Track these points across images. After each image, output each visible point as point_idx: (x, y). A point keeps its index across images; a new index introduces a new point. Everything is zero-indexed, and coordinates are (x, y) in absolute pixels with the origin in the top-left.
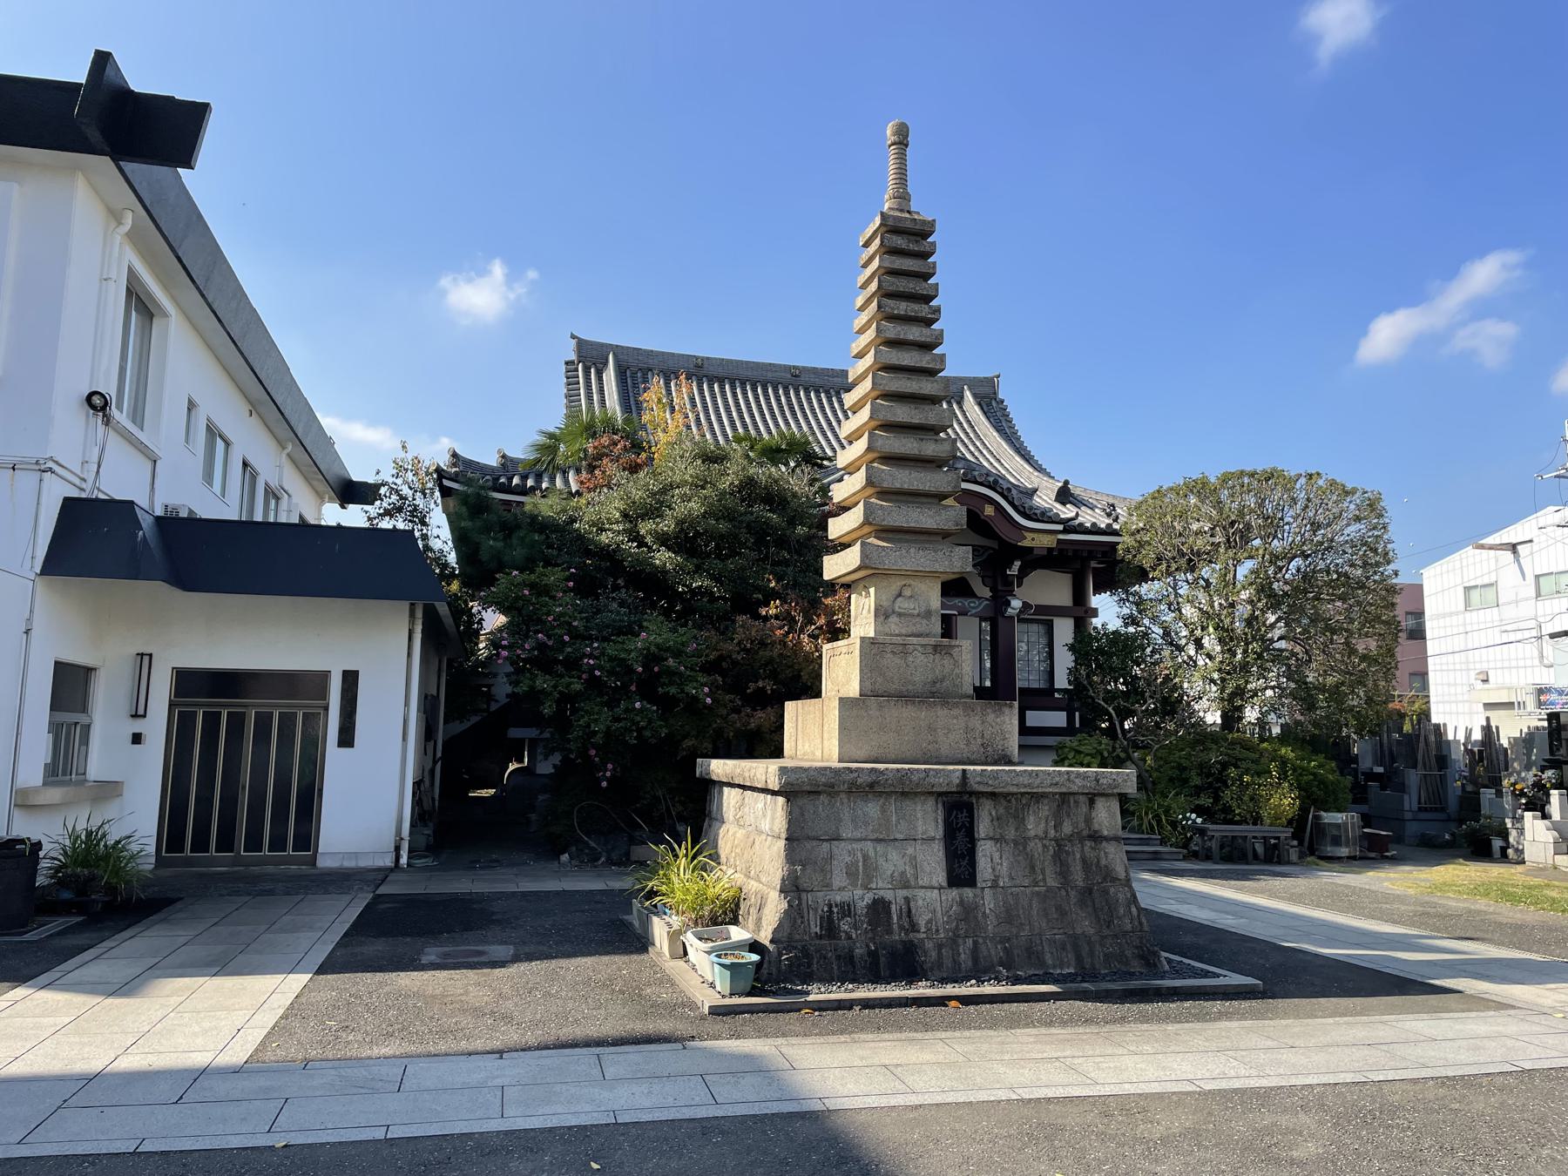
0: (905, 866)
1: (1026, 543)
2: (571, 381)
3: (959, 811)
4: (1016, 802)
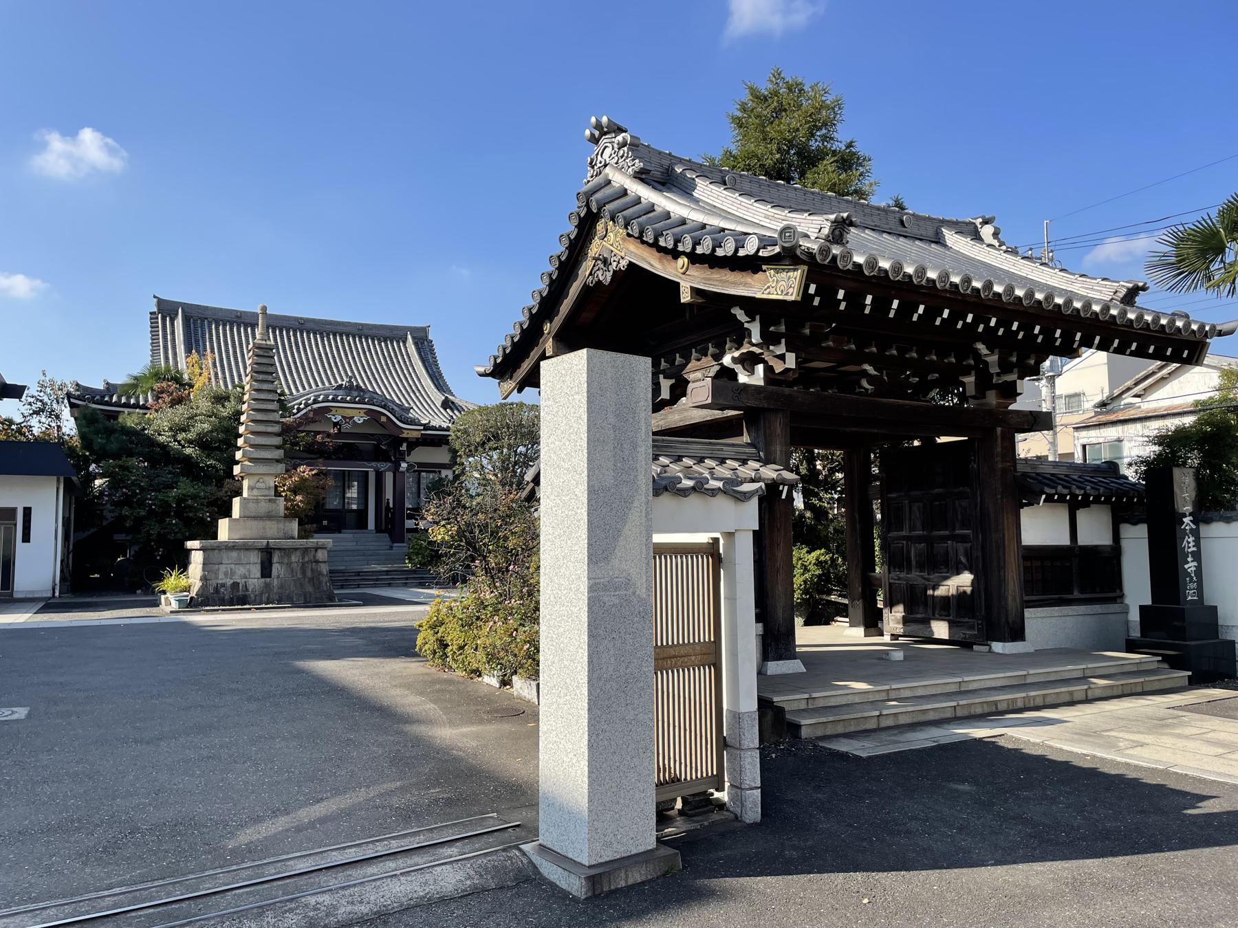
0: (248, 572)
1: (404, 435)
2: (154, 326)
3: (267, 554)
4: (287, 551)
